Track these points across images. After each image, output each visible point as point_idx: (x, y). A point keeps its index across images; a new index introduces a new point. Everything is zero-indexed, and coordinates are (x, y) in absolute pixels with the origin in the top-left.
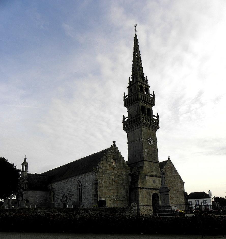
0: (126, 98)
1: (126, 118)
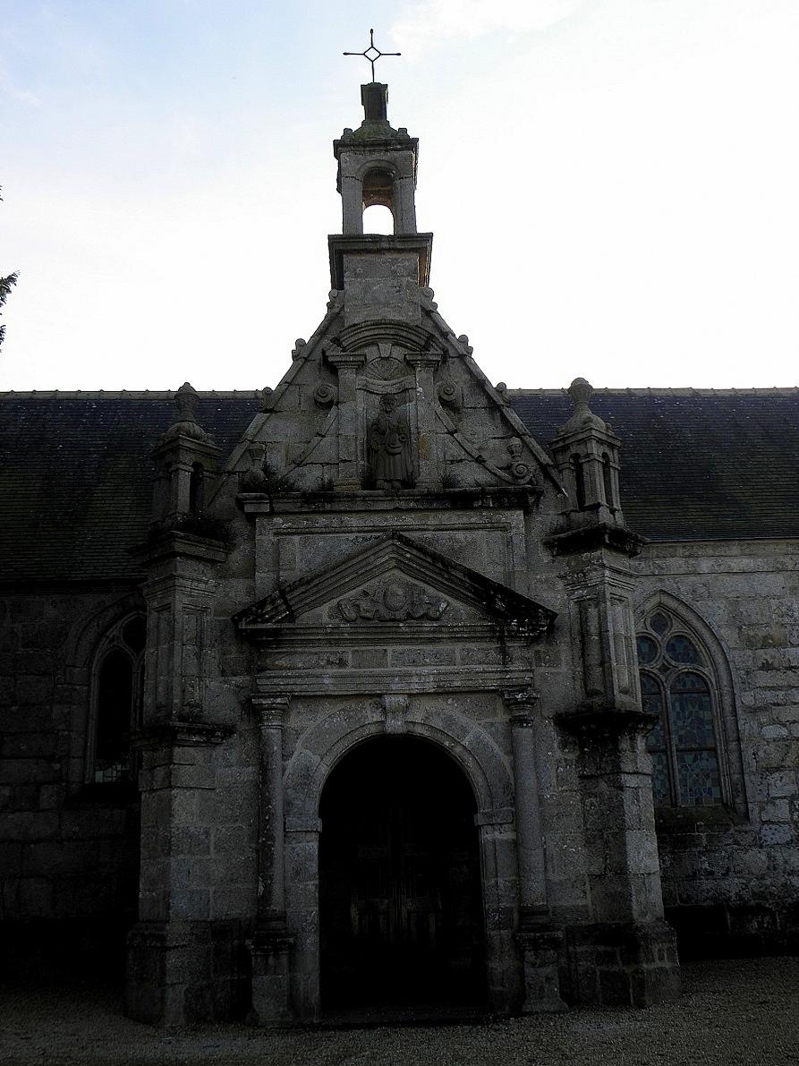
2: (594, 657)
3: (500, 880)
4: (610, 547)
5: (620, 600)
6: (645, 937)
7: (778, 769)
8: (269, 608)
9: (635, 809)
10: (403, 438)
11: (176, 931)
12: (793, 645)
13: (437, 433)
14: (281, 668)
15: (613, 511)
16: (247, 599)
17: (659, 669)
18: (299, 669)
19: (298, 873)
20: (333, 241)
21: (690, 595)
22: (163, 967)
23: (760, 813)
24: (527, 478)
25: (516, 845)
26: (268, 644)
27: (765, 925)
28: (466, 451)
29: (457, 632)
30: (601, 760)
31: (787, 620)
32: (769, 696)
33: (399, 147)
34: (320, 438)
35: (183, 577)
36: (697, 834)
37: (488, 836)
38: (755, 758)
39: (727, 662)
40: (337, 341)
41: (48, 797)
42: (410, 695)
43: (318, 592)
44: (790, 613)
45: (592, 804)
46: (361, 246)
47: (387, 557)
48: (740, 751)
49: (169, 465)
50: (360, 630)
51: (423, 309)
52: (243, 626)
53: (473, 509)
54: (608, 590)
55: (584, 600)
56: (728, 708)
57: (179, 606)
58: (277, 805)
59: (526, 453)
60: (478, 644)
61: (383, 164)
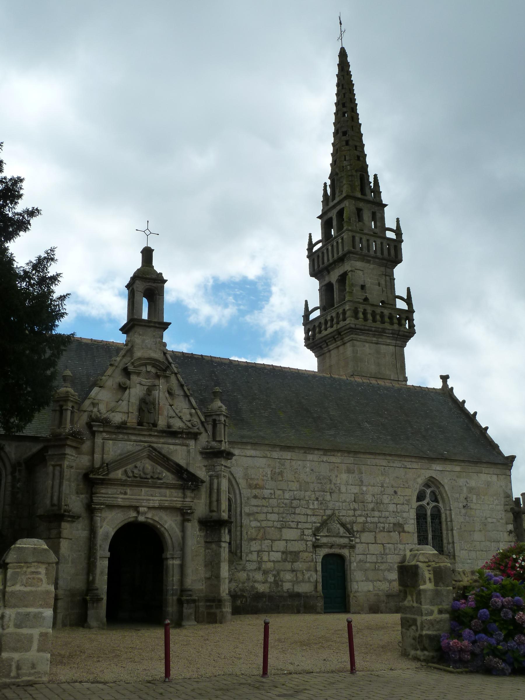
0: (315, 249)
1: (315, 309)
3: (174, 578)
7: (255, 539)
9: (224, 554)
12: (266, 489)
14: (103, 493)
18: (109, 494)
23: (246, 557)
24: (197, 427)
27: (243, 602)
31: (265, 478)
32: (255, 509)
33: (160, 282)
35: (68, 454)
44: (266, 475)
45: (208, 552)
54: (223, 473)
56: (238, 513)
59: (196, 417)
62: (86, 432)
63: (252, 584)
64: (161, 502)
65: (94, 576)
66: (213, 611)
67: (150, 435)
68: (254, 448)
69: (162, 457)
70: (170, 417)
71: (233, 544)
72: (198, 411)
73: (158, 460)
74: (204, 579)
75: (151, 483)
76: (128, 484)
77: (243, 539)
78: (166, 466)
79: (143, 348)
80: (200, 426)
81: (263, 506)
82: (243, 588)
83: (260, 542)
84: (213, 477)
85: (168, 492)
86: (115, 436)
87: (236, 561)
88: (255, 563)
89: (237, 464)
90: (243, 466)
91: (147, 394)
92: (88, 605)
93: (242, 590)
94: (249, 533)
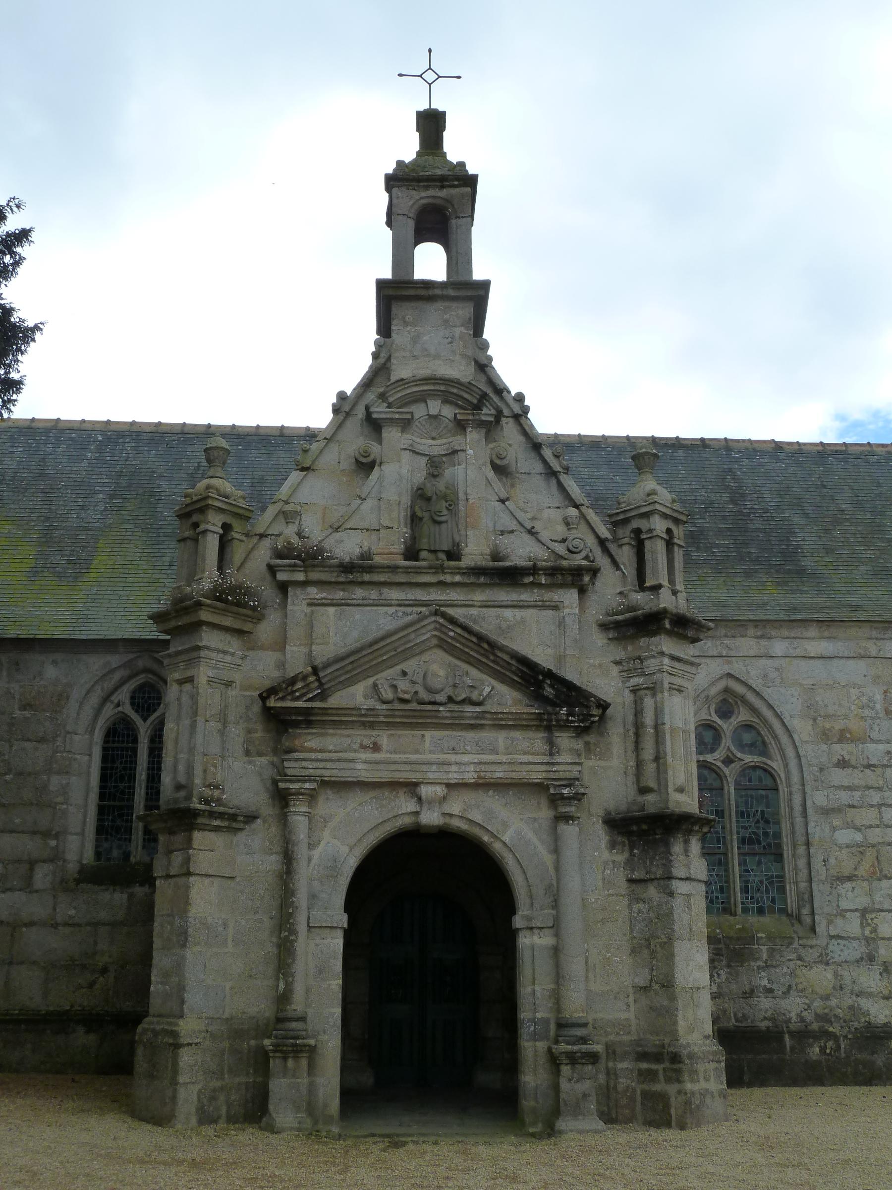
2: (648, 753)
3: (538, 988)
4: (670, 633)
5: (679, 691)
6: (691, 1056)
7: (850, 878)
8: (299, 685)
9: (686, 917)
10: (450, 505)
11: (187, 1027)
12: (873, 741)
13: (486, 501)
14: (311, 750)
15: (675, 593)
16: (276, 674)
17: (723, 762)
18: (330, 752)
19: (321, 972)
20: (381, 285)
21: (760, 681)
22: (175, 1064)
24: (583, 554)
25: (556, 951)
26: (296, 724)
27: (828, 1051)
28: (518, 521)
29: (502, 719)
30: (651, 863)
31: (867, 712)
32: (844, 797)
33: (456, 183)
34: (359, 501)
35: (207, 648)
36: (756, 946)
37: (524, 941)
38: (825, 865)
39: (798, 756)
40: (382, 396)
41: (42, 876)
42: (448, 785)
43: (354, 669)
44: (871, 705)
45: (640, 911)
46: (412, 292)
47: (428, 635)
48: (809, 856)
49: (196, 525)
50: (397, 713)
51: (476, 362)
52: (272, 703)
53: (525, 585)
54: (667, 679)
55: (640, 689)
56: (798, 808)
57: (202, 680)
58: (301, 898)
59: (583, 527)
60: (523, 732)
61: (438, 202)
62: (268, 592)
63: (850, 1002)
64: (483, 767)
65: (291, 979)
66: (658, 1087)
67: (441, 584)
68: (826, 634)
69: (474, 639)
70: (502, 533)
71: (791, 891)
72: (591, 515)
73: (466, 650)
74: (631, 991)
75: (448, 714)
76: (383, 722)
77: (814, 879)
78: (492, 665)
79: (415, 357)
80: (598, 552)
81: (868, 787)
82: (826, 1011)
83: (865, 884)
84: (642, 692)
85: (501, 738)
86: (341, 593)
87: (799, 938)
88: (855, 944)
89: (782, 678)
90: (801, 685)
91: (429, 474)
92: (271, 1061)
93: (824, 1018)
94: (830, 860)
